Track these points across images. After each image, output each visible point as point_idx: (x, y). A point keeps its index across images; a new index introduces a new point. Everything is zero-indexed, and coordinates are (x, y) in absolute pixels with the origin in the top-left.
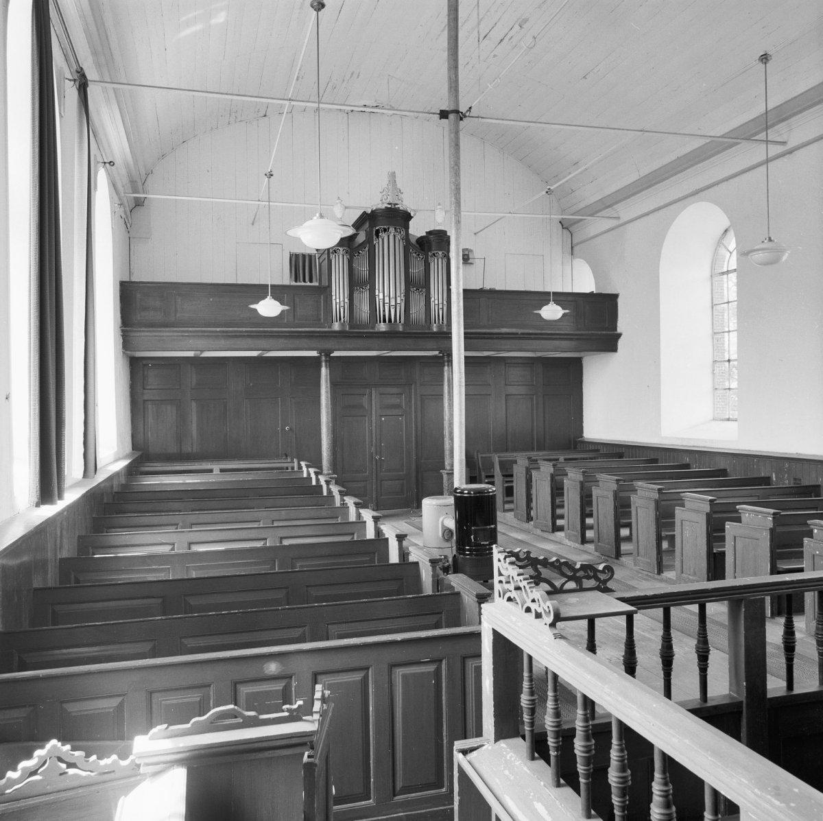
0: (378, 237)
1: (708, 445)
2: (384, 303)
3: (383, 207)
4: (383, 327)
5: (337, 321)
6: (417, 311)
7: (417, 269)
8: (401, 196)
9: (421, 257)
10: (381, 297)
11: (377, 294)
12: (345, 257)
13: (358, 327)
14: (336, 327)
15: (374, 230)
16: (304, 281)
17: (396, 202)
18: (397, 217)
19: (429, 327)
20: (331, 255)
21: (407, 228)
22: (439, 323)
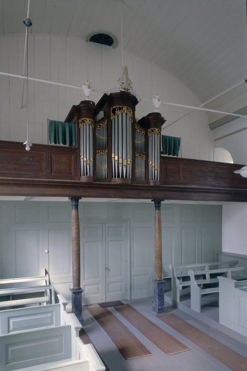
0: (114, 114)
1: (97, 358)
2: (152, 166)
3: (119, 91)
4: (117, 181)
5: (84, 175)
6: (140, 171)
7: (140, 141)
8: (131, 85)
9: (143, 133)
10: (116, 158)
11: (113, 156)
12: (91, 126)
13: (100, 180)
14: (84, 179)
15: (112, 108)
16: (59, 143)
17: (128, 88)
18: (127, 100)
19: (148, 183)
20: (80, 124)
21: (134, 111)
22: (155, 179)
